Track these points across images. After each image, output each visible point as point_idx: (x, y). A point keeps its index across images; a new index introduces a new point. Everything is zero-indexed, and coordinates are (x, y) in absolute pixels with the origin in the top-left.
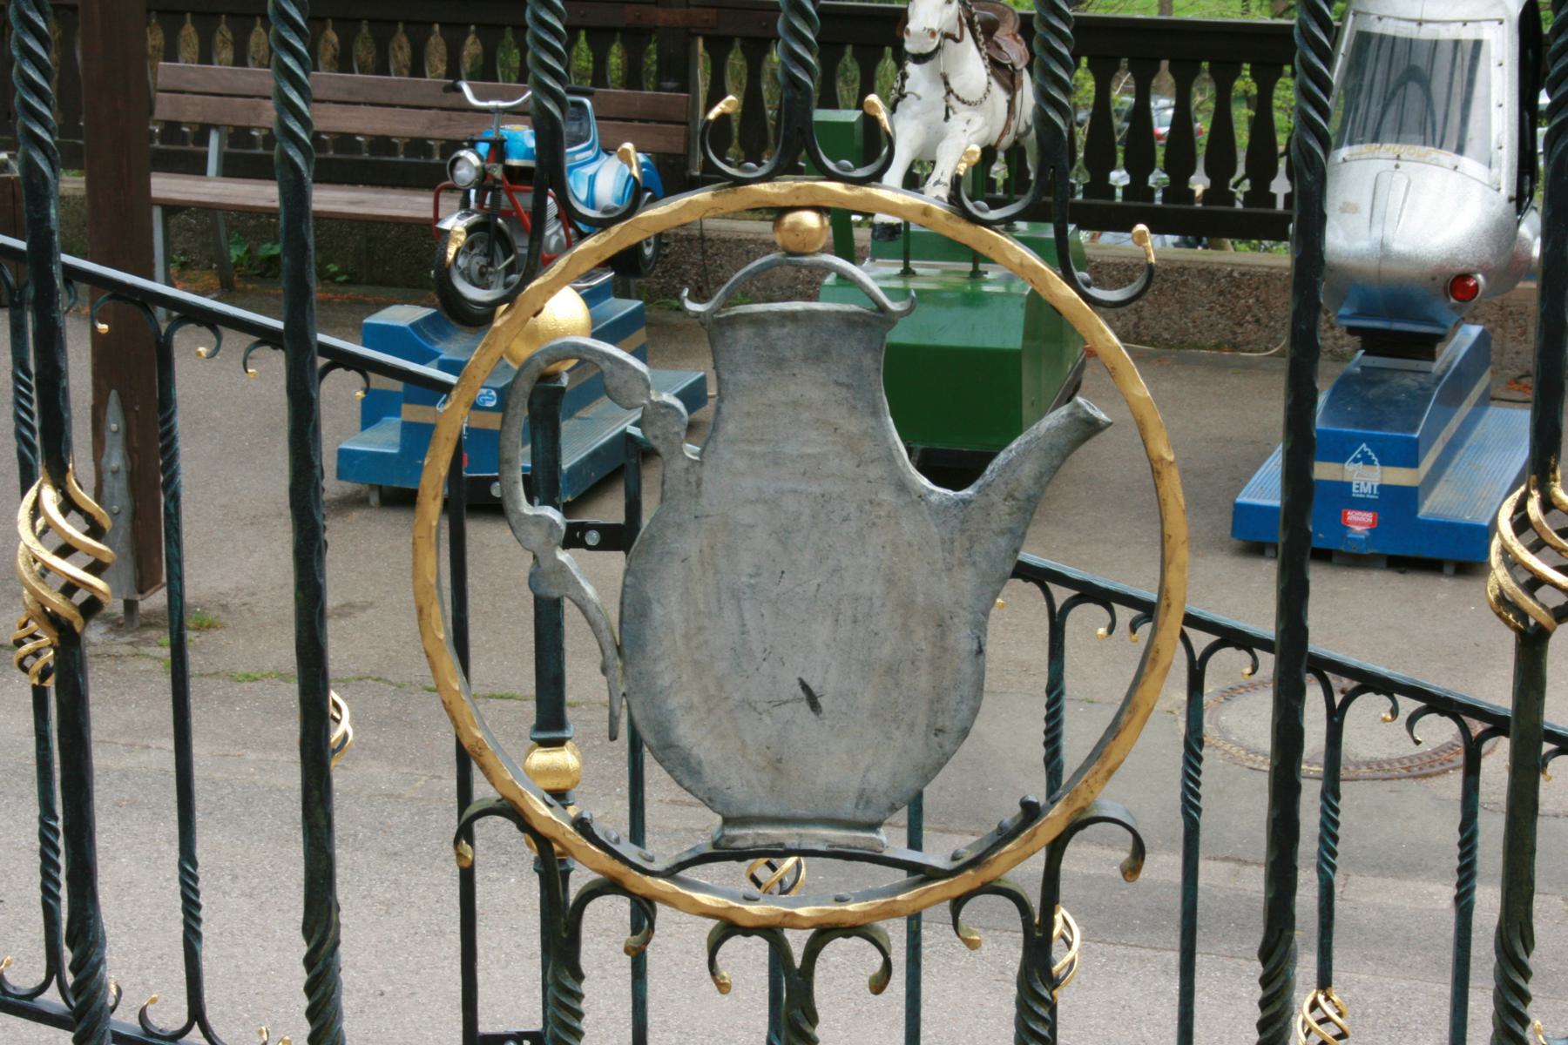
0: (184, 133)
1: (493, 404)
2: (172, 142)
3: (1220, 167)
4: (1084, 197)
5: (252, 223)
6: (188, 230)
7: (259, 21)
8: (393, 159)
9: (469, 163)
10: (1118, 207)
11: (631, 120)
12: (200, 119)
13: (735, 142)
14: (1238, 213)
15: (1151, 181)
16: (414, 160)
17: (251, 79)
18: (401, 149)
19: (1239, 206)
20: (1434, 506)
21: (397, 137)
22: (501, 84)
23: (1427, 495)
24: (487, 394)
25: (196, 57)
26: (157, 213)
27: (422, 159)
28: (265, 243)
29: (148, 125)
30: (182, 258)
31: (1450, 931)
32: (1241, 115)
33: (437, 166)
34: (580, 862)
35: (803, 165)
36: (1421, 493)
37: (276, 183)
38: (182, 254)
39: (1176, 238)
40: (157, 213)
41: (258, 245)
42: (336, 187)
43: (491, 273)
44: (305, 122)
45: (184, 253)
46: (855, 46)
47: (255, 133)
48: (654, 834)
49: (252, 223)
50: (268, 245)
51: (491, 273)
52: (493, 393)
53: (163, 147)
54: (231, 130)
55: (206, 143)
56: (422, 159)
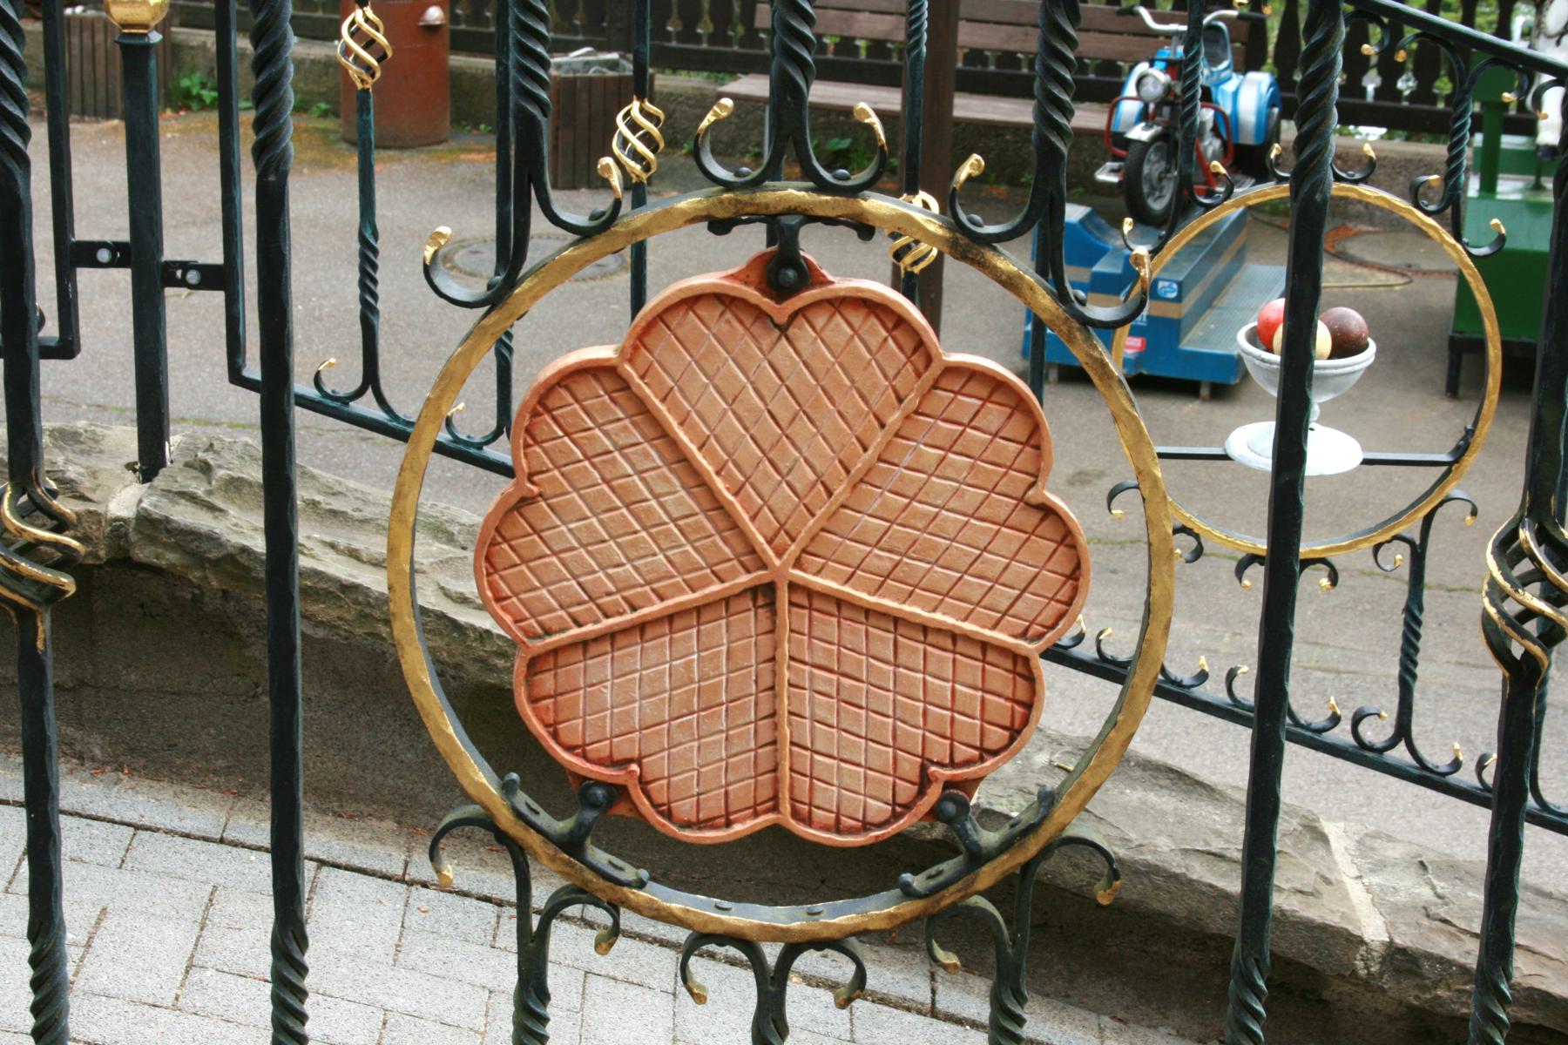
1: (1174, 295)
2: (750, 47)
4: (959, 72)
5: (822, 120)
9: (1156, 79)
13: (1270, 61)
15: (1400, 85)
16: (972, 68)
18: (992, 59)
20: (1193, 342)
21: (989, 50)
23: (1190, 327)
24: (1170, 286)
27: (979, 68)
33: (894, 67)
34: (71, 814)
36: (1183, 324)
39: (1383, 131)
41: (827, 139)
43: (1168, 171)
44: (1072, 43)
48: (1549, 758)
49: (822, 120)
51: (1168, 171)
52: (1175, 286)
53: (743, 51)
54: (966, 50)
56: (979, 68)
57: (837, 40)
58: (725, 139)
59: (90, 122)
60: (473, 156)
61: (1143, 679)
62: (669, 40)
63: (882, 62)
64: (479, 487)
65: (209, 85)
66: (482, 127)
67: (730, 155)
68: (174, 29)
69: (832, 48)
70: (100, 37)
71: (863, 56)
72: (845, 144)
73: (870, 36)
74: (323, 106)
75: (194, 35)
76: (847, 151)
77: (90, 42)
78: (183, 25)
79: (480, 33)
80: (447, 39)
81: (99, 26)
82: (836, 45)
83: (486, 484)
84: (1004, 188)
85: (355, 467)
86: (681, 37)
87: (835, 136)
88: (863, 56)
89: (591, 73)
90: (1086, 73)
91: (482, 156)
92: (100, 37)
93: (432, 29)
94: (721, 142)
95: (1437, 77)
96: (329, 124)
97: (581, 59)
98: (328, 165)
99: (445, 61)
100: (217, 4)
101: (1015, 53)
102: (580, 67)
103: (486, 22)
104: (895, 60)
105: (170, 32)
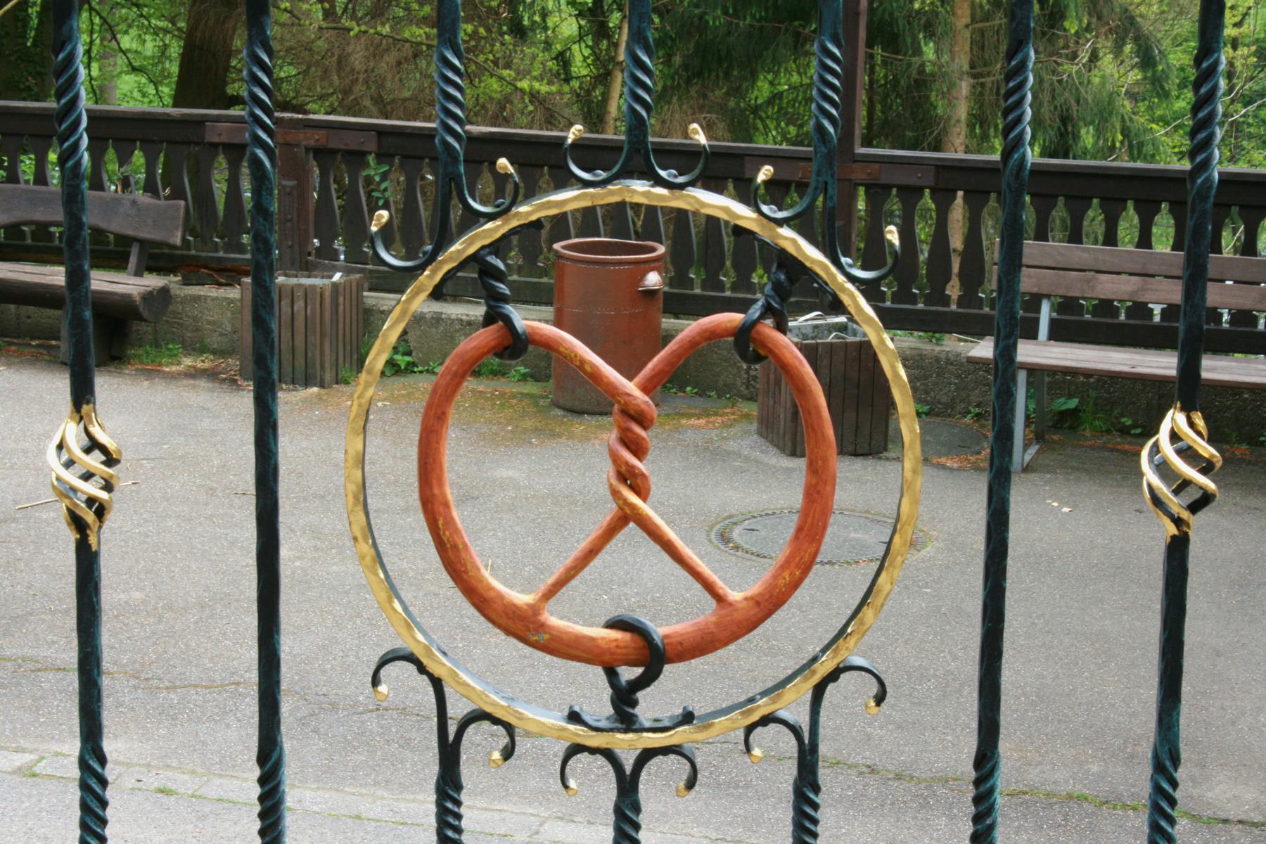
0: (981, 298)
2: (1105, 316)
3: (973, 273)
6: (985, 385)
7: (993, 196)
8: (946, 309)
10: (1156, 327)
11: (1119, 273)
12: (1035, 290)
14: (1121, 325)
17: (1086, 255)
19: (1122, 317)
22: (1050, 243)
25: (1067, 239)
26: (1022, 377)
27: (1212, 326)
28: (1059, 398)
29: (718, 275)
30: (977, 410)
31: (109, 717)
32: (923, 232)
35: (917, 292)
37: (1176, 354)
38: (976, 406)
40: (1022, 377)
42: (1118, 348)
45: (978, 406)
46: (966, 192)
47: (53, 229)
50: (1063, 400)
55: (1038, 311)
57: (34, 227)
58: (944, 400)
59: (289, 390)
60: (693, 421)
61: (627, 745)
62: (216, 251)
63: (1110, 321)
64: (887, 807)
65: (401, 349)
66: (689, 389)
67: (950, 416)
68: (365, 294)
69: (728, 285)
70: (299, 305)
71: (1157, 319)
72: (1073, 403)
73: (1168, 302)
74: (522, 370)
75: (383, 299)
76: (1074, 413)
77: (289, 310)
78: (370, 290)
79: (686, 294)
80: (660, 303)
81: (300, 293)
82: (1163, 311)
83: (892, 804)
84: (1244, 447)
85: (747, 786)
86: (734, 288)
87: (1061, 396)
88: (1157, 319)
89: (831, 338)
90: (884, 301)
91: (702, 422)
92: (299, 305)
93: (651, 293)
94: (939, 402)
95: (754, 269)
96: (530, 388)
97: (810, 323)
98: (554, 435)
99: (659, 324)
100: (1261, 333)
101: (1112, 301)
102: (809, 331)
103: (241, 248)
104: (987, 310)
105: (363, 297)
